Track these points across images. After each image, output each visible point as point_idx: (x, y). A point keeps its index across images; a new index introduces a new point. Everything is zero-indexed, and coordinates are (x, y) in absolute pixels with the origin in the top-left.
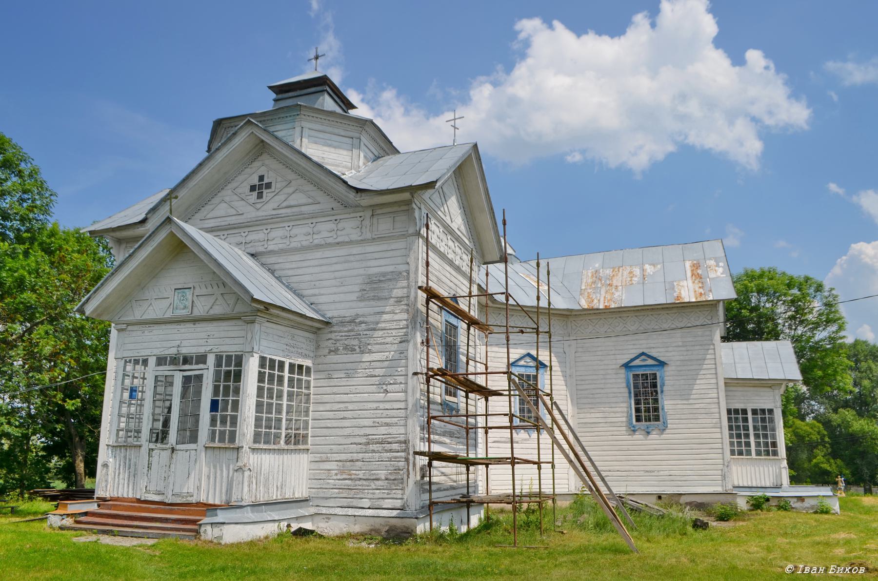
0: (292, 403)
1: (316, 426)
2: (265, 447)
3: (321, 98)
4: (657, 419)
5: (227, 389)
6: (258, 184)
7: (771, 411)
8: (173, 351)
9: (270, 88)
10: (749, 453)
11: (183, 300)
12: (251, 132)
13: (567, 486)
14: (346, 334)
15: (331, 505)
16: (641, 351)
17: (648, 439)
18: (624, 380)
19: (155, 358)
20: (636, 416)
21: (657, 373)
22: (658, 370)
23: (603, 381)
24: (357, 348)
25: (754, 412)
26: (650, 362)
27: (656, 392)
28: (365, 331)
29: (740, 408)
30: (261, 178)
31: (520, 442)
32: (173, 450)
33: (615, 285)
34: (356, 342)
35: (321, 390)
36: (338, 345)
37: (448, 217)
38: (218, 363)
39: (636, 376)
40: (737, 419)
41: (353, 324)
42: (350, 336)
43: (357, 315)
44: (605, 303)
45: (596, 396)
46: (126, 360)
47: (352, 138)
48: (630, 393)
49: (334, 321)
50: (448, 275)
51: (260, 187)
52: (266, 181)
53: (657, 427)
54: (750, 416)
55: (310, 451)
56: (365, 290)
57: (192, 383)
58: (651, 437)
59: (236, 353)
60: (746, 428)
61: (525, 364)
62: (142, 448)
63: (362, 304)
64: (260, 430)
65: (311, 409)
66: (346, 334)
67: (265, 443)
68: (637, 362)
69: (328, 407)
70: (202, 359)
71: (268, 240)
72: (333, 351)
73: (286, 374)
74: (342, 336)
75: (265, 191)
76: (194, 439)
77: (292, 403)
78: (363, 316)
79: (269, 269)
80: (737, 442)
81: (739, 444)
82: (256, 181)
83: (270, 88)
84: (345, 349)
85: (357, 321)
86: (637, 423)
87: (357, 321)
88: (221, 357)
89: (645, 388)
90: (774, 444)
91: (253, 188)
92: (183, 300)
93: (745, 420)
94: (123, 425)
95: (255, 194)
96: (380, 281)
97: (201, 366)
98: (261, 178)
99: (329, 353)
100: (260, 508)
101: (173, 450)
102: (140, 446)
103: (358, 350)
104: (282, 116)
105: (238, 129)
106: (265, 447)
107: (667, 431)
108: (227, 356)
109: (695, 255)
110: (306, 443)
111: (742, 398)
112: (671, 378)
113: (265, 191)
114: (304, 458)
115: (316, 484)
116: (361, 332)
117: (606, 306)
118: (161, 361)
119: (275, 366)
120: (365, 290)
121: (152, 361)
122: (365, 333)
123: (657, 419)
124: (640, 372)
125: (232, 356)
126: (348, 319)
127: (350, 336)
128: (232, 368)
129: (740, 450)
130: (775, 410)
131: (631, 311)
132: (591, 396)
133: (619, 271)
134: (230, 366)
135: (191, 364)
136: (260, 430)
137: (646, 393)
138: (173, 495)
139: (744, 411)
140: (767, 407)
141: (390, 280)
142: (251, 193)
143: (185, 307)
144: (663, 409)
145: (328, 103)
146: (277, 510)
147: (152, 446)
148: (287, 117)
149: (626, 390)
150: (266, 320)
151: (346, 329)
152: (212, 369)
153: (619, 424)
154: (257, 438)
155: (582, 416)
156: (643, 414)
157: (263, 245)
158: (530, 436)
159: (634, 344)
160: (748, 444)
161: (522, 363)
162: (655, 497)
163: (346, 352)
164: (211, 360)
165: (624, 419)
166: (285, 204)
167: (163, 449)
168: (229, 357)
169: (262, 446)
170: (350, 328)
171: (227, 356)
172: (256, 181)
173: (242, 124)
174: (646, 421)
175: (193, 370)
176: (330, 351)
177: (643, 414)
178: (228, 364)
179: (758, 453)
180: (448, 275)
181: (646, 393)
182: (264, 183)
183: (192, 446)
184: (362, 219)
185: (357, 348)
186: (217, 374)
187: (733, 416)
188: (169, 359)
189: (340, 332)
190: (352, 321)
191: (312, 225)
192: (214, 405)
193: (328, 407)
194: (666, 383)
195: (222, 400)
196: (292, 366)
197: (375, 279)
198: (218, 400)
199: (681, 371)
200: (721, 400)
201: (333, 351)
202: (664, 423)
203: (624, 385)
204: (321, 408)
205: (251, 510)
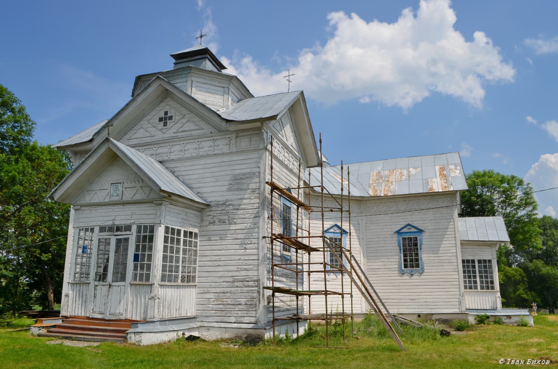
0: (186, 256)
1: (201, 270)
2: (169, 284)
3: (204, 62)
4: (418, 266)
5: (144, 247)
6: (164, 117)
7: (490, 261)
8: (110, 223)
9: (172, 56)
10: (476, 288)
11: (116, 190)
12: (159, 84)
13: (360, 309)
14: (220, 212)
15: (210, 321)
16: (407, 223)
17: (412, 279)
18: (396, 242)
19: (98, 227)
20: (404, 264)
21: (418, 237)
22: (418, 235)
23: (383, 242)
24: (227, 221)
25: (479, 261)
26: (413, 230)
27: (417, 249)
28: (232, 210)
29: (470, 259)
30: (166, 113)
31: (330, 281)
32: (110, 286)
33: (391, 181)
34: (226, 217)
35: (204, 248)
36: (215, 219)
37: (285, 138)
38: (139, 231)
39: (404, 239)
40: (468, 266)
41: (224, 206)
42: (222, 213)
43: (227, 200)
44: (384, 192)
45: (379, 251)
46: (80, 229)
47: (224, 88)
48: (400, 249)
49: (212, 204)
50: (285, 175)
51: (165, 119)
52: (169, 115)
53: (417, 271)
54: (477, 264)
55: (197, 287)
56: (232, 184)
57: (122, 244)
58: (413, 277)
59: (150, 224)
60: (474, 272)
61: (334, 231)
62: (90, 285)
63: (230, 193)
64: (165, 273)
65: (198, 260)
66: (220, 212)
67: (168, 281)
68: (405, 230)
69: (208, 258)
70: (128, 228)
71: (170, 152)
72: (211, 223)
73: (182, 238)
74: (217, 213)
75: (168, 122)
76: (123, 279)
77: (186, 256)
78: (231, 200)
79: (171, 171)
80: (469, 281)
81: (470, 282)
82: (162, 115)
83: (172, 56)
84: (219, 221)
85: (227, 204)
86: (405, 269)
87: (227, 204)
88: (141, 227)
89: (410, 246)
90: (492, 282)
91: (161, 120)
92: (116, 190)
93: (474, 267)
94: (78, 270)
95: (162, 123)
96: (242, 179)
97: (128, 232)
98: (166, 113)
99: (209, 224)
100: (165, 322)
101: (110, 286)
102: (89, 284)
103: (227, 222)
104: (179, 73)
105: (152, 82)
106: (169, 284)
107: (424, 274)
108: (144, 226)
109: (442, 162)
110: (195, 281)
111: (472, 253)
112: (426, 240)
113: (168, 122)
114: (193, 291)
115: (201, 307)
116: (230, 211)
117: (385, 194)
118: (102, 229)
119: (175, 233)
120: (232, 184)
121: (97, 229)
122: (232, 211)
123: (418, 266)
124: (407, 236)
125: (147, 226)
126: (221, 203)
127: (222, 213)
128: (148, 234)
129: (470, 286)
130: (492, 260)
131: (401, 197)
132: (376, 251)
133: (393, 172)
134: (146, 232)
135: (121, 231)
136: (165, 273)
137: (410, 250)
138: (110, 314)
139: (473, 261)
140: (487, 258)
141: (248, 178)
142: (160, 123)
143: (118, 195)
144: (421, 260)
145: (208, 65)
146: (176, 324)
147: (97, 283)
148: (182, 74)
149: (398, 248)
150: (169, 203)
151: (220, 209)
152: (135, 234)
153: (393, 269)
154: (163, 278)
155: (370, 264)
156: (409, 263)
157: (167, 156)
158: (337, 277)
159: (403, 219)
160: (475, 282)
161: (332, 230)
162: (417, 315)
163: (220, 224)
164: (134, 228)
165: (397, 266)
166: (181, 130)
167: (104, 285)
168: (146, 227)
169: (173, 284)
170: (222, 208)
171: (144, 226)
172: (162, 115)
173: (154, 79)
174: (410, 267)
175: (123, 235)
176: (210, 223)
177: (409, 263)
178: (145, 231)
179: (482, 288)
180: (285, 175)
181: (410, 250)
182: (168, 116)
183: (122, 283)
184: (230, 139)
185: (227, 221)
186: (138, 237)
187: (466, 264)
188: (107, 228)
189: (216, 211)
190: (224, 204)
191: (199, 143)
192: (136, 257)
193: (208, 258)
194: (424, 243)
195: (141, 254)
196: (185, 232)
197: (238, 177)
198: (139, 254)
199: (433, 235)
200: (458, 254)
201: (211, 223)
202: (422, 268)
203: (397, 244)
204: (204, 259)
205: (160, 324)
